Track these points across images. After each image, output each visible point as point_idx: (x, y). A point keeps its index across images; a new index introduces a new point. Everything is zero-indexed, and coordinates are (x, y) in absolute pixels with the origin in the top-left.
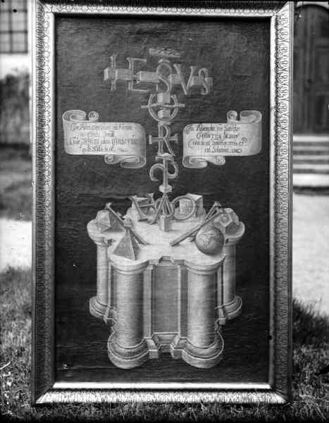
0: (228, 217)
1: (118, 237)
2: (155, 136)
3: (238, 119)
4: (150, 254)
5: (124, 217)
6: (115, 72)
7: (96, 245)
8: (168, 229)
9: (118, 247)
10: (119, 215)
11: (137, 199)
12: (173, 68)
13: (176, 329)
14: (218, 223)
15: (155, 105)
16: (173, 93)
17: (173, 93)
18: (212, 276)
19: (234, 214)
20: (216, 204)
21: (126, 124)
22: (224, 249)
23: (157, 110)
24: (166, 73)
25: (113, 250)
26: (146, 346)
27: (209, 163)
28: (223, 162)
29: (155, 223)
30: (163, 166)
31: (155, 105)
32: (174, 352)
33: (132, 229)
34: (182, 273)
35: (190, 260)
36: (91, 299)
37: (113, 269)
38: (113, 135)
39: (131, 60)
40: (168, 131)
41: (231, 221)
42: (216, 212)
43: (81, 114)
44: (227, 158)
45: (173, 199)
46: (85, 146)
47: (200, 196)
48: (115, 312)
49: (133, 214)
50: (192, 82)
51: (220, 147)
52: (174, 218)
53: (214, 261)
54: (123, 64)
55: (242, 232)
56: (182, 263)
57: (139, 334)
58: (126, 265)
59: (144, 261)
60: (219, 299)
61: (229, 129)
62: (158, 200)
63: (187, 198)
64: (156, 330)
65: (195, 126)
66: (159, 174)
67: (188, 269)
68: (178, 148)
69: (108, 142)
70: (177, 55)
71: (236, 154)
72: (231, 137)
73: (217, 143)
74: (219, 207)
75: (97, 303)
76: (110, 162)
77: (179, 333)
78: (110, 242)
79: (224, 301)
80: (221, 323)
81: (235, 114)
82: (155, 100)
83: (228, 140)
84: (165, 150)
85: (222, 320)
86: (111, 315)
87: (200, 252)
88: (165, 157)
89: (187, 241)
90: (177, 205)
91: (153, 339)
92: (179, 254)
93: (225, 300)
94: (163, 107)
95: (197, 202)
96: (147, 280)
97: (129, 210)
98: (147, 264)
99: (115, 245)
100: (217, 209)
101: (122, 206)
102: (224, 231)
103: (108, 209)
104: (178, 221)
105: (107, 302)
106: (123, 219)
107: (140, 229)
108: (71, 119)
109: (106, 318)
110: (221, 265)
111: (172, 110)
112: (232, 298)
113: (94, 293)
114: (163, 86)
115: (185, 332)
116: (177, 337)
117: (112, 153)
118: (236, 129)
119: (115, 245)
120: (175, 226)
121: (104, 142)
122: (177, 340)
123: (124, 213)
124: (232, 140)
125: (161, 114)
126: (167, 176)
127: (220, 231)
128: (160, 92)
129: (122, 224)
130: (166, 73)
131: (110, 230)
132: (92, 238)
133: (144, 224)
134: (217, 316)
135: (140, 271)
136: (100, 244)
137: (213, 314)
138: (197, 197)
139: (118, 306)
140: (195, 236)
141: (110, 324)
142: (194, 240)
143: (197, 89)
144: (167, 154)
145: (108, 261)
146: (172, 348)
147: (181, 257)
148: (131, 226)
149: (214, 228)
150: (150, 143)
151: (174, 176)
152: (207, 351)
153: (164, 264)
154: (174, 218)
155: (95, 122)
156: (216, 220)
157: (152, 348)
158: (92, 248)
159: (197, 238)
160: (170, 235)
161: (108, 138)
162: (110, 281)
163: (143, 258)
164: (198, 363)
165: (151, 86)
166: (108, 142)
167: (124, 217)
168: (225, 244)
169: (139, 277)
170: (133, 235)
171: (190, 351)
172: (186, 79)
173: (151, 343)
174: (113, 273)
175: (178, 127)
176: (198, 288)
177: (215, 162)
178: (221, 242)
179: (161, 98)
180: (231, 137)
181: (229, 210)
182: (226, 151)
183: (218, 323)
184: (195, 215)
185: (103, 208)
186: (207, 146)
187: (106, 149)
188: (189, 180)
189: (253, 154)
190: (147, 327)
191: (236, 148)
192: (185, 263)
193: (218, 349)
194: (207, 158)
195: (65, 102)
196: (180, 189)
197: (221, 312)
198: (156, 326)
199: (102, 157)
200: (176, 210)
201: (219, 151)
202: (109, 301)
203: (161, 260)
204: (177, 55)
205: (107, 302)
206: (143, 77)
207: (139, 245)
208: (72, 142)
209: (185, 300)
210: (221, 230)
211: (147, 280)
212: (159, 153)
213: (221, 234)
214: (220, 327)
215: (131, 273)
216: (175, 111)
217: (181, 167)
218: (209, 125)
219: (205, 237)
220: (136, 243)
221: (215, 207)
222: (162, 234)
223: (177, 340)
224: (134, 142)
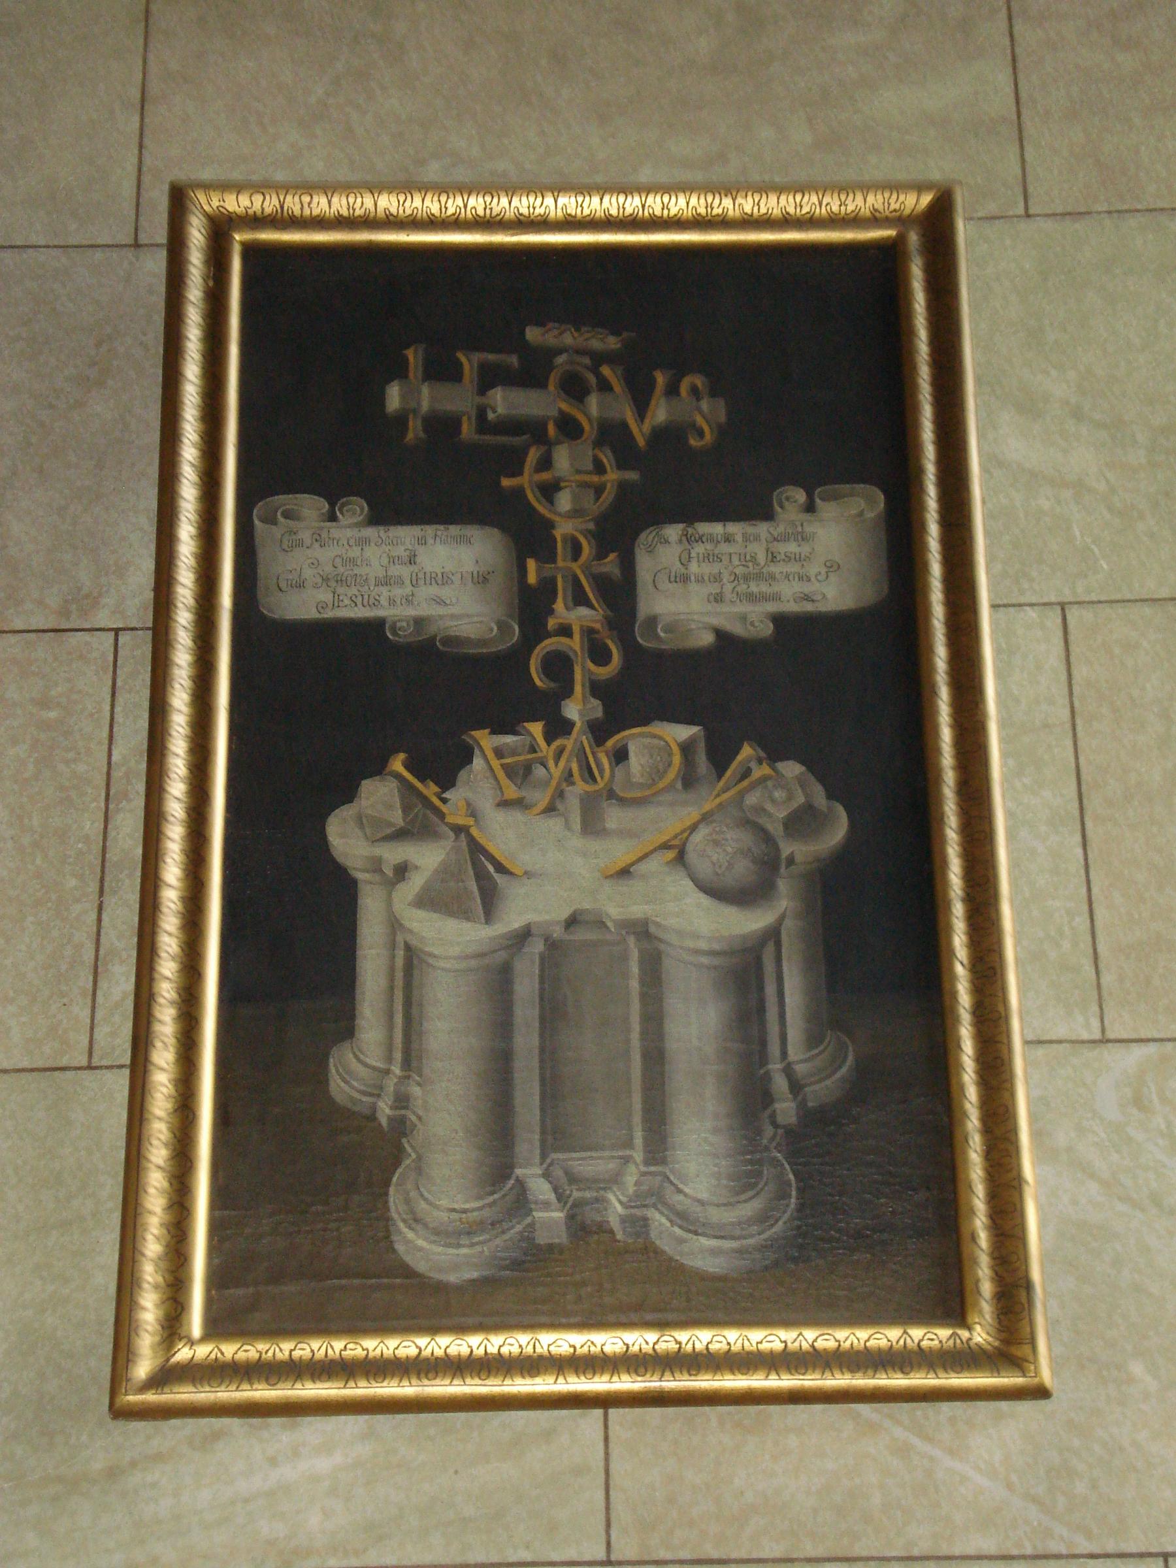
0: (782, 787)
1: (428, 858)
2: (546, 553)
3: (810, 508)
4: (529, 907)
5: (446, 795)
6: (419, 392)
7: (354, 882)
8: (591, 825)
9: (426, 888)
10: (430, 790)
11: (486, 740)
12: (598, 375)
13: (629, 1144)
14: (760, 810)
15: (545, 476)
16: (598, 443)
17: (598, 443)
18: (744, 975)
19: (812, 779)
20: (747, 751)
21: (454, 530)
22: (782, 885)
23: (549, 491)
24: (574, 388)
25: (410, 898)
26: (521, 1203)
27: (720, 634)
28: (766, 630)
29: (550, 809)
30: (575, 644)
31: (545, 476)
32: (624, 1220)
33: (474, 832)
34: (642, 962)
35: (672, 922)
36: (334, 1051)
37: (408, 948)
38: (412, 560)
39: (469, 362)
40: (587, 550)
41: (800, 799)
42: (747, 773)
43: (311, 506)
44: (779, 620)
45: (605, 741)
46: (325, 596)
47: (693, 730)
48: (416, 1091)
49: (477, 788)
50: (660, 413)
51: (754, 588)
52: (611, 794)
53: (749, 922)
54: (442, 370)
55: (838, 831)
56: (642, 930)
57: (498, 1169)
58: (453, 941)
59: (516, 925)
60: (774, 1049)
61: (784, 538)
62: (558, 743)
63: (655, 736)
64: (557, 1149)
65: (673, 532)
66: (558, 666)
67: (662, 947)
68: (620, 595)
69: (400, 582)
70: (613, 343)
71: (809, 607)
72: (788, 558)
73: (747, 578)
74: (760, 761)
75: (355, 1065)
76: (406, 634)
77: (638, 1155)
78: (402, 871)
79: (791, 1050)
80: (780, 1119)
81: (801, 496)
82: (546, 463)
83: (775, 569)
84: (580, 599)
85: (786, 1109)
86: (402, 1101)
87: (702, 895)
88: (579, 618)
89: (654, 865)
90: (621, 756)
91: (546, 1175)
92: (618, 905)
93: (795, 1052)
94: (571, 487)
95: (687, 749)
96: (526, 987)
97: (463, 775)
98: (524, 935)
99: (416, 883)
100: (753, 765)
101: (443, 764)
102: (776, 829)
103: (398, 776)
104: (623, 801)
105: (389, 1059)
106: (444, 801)
107: (503, 833)
108: (281, 519)
109: (385, 1110)
110: (773, 934)
111: (599, 490)
112: (813, 1040)
113: (347, 1031)
114: (570, 428)
115: (658, 1145)
116: (632, 1168)
117: (411, 612)
118: (803, 538)
119: (416, 883)
120: (614, 817)
121: (386, 581)
122: (630, 1179)
123: (447, 782)
124: (793, 568)
125: (564, 501)
126: (583, 670)
127: (764, 830)
128: (559, 442)
129: (442, 816)
130: (574, 388)
131: (400, 835)
132: (341, 860)
133: (517, 816)
134: (768, 1098)
135: (502, 956)
136: (367, 876)
137: (750, 1098)
138: (683, 732)
139: (426, 1071)
140: (684, 844)
141: (401, 1127)
142: (681, 858)
143: (669, 437)
144: (583, 611)
145: (394, 925)
146: (616, 1207)
147: (638, 910)
148: (470, 821)
149: (748, 823)
150: (532, 579)
151: (603, 672)
152: (728, 1216)
153: (581, 935)
154: (611, 794)
155: (358, 525)
156: (751, 799)
157: (546, 1205)
158: (343, 889)
159: (691, 856)
160: (594, 845)
161: (396, 570)
162: (399, 975)
163: (512, 919)
164: (704, 1255)
165: (534, 430)
166: (400, 582)
167: (446, 795)
168: (783, 870)
169: (498, 982)
170: (477, 849)
171: (682, 1218)
172: (641, 409)
173: (541, 1189)
174: (411, 963)
175: (619, 531)
176: (697, 1024)
177: (738, 629)
178: (769, 865)
179: (563, 459)
180: (788, 558)
181: (792, 769)
182: (776, 597)
183: (773, 1116)
184: (679, 785)
185: (378, 768)
186: (712, 583)
187: (392, 602)
188: (653, 682)
189: (861, 605)
190: (527, 1143)
191: (807, 588)
192: (652, 929)
193: (763, 1218)
194: (715, 621)
195: (1005, 1262)
196: (623, 708)
197: (780, 1084)
198: (556, 1137)
199: (378, 625)
200: (619, 771)
201: (752, 598)
202: (398, 1056)
203: (572, 921)
204: (613, 343)
205: (389, 1059)
206: (503, 402)
207: (496, 875)
208: (283, 585)
209: (656, 1057)
210: (769, 827)
211: (526, 987)
212: (559, 606)
213: (767, 838)
214: (780, 1131)
215: (473, 963)
216: (608, 496)
217: (631, 649)
218: (717, 529)
219: (723, 851)
220: (482, 879)
221: (749, 759)
222: (576, 841)
223: (630, 1179)
224: (482, 580)
